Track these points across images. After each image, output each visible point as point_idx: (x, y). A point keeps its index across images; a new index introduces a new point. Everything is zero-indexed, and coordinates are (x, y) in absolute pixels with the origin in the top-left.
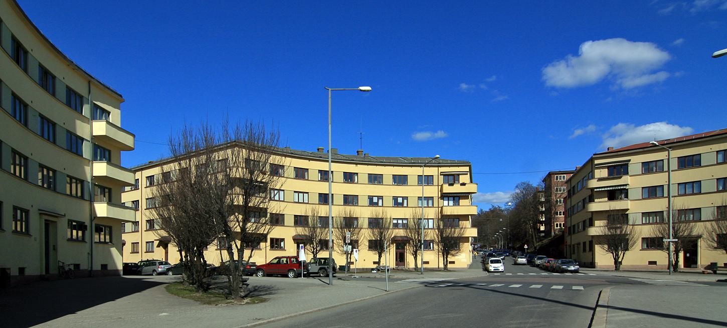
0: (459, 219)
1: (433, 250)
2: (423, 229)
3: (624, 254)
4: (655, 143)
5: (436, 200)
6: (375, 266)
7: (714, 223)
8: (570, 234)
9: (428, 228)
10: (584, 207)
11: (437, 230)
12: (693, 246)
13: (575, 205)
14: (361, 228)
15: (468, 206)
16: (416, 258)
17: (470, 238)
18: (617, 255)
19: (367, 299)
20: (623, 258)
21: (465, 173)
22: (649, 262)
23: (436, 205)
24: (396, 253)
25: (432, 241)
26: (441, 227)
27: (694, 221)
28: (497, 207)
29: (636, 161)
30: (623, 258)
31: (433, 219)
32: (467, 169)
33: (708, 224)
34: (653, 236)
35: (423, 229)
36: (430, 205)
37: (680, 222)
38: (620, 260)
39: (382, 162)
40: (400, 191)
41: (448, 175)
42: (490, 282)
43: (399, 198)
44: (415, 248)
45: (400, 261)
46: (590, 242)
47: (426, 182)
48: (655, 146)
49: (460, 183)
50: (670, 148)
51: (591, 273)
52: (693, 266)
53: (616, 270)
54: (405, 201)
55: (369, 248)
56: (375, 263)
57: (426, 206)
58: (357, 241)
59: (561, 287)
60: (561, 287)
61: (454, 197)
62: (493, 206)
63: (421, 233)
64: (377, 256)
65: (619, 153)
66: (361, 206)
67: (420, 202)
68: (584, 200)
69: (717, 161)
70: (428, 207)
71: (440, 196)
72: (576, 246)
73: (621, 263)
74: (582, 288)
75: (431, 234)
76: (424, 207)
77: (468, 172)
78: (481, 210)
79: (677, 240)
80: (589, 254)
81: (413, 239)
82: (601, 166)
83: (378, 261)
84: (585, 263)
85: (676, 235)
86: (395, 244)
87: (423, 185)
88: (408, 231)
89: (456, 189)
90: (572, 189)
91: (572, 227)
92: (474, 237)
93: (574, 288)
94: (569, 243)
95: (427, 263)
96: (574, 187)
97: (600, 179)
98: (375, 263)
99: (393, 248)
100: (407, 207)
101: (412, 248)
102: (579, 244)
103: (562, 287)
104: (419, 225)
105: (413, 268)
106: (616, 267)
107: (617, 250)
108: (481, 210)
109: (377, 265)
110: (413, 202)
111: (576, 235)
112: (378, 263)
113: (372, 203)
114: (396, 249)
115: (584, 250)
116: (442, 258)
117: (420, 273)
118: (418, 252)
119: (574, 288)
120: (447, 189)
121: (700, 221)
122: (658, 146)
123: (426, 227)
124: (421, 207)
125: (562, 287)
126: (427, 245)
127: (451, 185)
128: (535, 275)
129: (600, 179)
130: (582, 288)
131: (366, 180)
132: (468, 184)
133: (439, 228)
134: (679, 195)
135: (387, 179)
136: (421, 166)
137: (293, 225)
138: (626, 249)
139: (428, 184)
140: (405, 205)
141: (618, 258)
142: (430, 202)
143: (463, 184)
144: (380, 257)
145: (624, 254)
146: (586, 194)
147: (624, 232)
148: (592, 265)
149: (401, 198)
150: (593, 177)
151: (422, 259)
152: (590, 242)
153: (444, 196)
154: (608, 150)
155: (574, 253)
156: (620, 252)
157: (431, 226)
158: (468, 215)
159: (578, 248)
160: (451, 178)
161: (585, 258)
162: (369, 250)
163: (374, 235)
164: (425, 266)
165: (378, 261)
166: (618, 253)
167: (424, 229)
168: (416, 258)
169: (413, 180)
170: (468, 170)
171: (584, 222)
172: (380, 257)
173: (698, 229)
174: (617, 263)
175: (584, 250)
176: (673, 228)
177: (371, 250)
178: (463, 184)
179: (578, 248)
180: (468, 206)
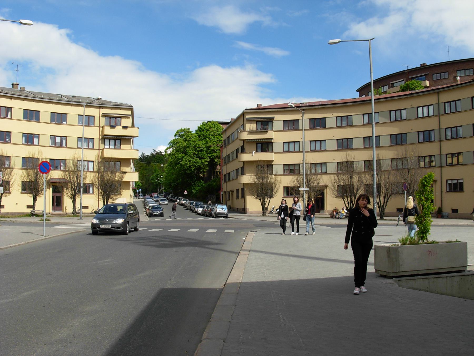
0: (120, 162)
1: (93, 194)
2: (82, 171)
3: (269, 201)
4: (292, 105)
5: (96, 141)
6: (29, 211)
7: (335, 176)
8: (225, 181)
9: (88, 171)
10: (237, 157)
11: (97, 174)
12: (321, 194)
13: (229, 154)
14: (13, 169)
15: (130, 150)
16: (74, 202)
17: (131, 183)
18: (264, 201)
19: (22, 244)
20: (268, 205)
21: (127, 117)
22: (397, 209)
23: (96, 146)
24: (53, 197)
25: (92, 184)
26: (102, 170)
27: (322, 174)
28: (158, 152)
29: (279, 119)
30: (268, 205)
31: (93, 161)
32: (129, 112)
33: (332, 176)
34: (293, 185)
35: (82, 171)
36: (91, 146)
37: (311, 174)
38: (266, 206)
39: (40, 98)
40: (58, 130)
41: (110, 117)
42: (169, 227)
43: (57, 138)
44: (73, 191)
45: (57, 205)
46: (242, 189)
47: (87, 123)
48: (291, 107)
49: (122, 125)
50: (304, 110)
51: (242, 217)
52: (321, 211)
53: (263, 215)
54: (64, 142)
55: (22, 190)
56: (28, 207)
57: (86, 147)
58: (8, 182)
59: (214, 231)
60: (214, 231)
61: (115, 140)
62: (155, 151)
63: (80, 176)
64: (32, 199)
65: (265, 110)
66: (363, 161)
67: (80, 143)
68: (237, 150)
69: (337, 125)
70: (88, 149)
71: (100, 137)
72: (230, 192)
73: (267, 208)
74: (232, 231)
75: (90, 178)
76: (84, 149)
77: (130, 115)
78: (143, 154)
79: (309, 189)
80: (241, 200)
81: (71, 182)
82: (250, 120)
83: (32, 204)
84: (238, 209)
85: (308, 185)
86: (51, 189)
87: (84, 125)
88: (67, 173)
89: (118, 131)
90: (227, 139)
91: (227, 175)
92: (135, 182)
93: (226, 231)
94: (224, 190)
95: (86, 207)
96: (229, 138)
97: (251, 132)
98: (28, 207)
99: (49, 192)
100: (66, 147)
101: (70, 191)
102: (233, 191)
103: (217, 230)
104: (78, 167)
105: (71, 213)
106: (263, 213)
107: (264, 199)
108: (143, 154)
109: (32, 209)
110: (72, 142)
111: (230, 182)
112: (33, 207)
113: (54, 144)
114: (52, 192)
115: (238, 197)
116: (102, 202)
117: (79, 218)
118: (77, 196)
119: (226, 231)
120: (108, 131)
121: (326, 173)
122: (294, 108)
123: (86, 169)
124: (81, 148)
125: (217, 230)
126: (86, 189)
127: (113, 127)
128: (192, 220)
129: (251, 132)
130: (232, 231)
131: (21, 116)
132: (130, 127)
133: (99, 171)
134: (311, 151)
135: (45, 117)
136: (81, 106)
137: (21, 167)
138: (271, 197)
139: (89, 124)
140: (64, 145)
141: (265, 204)
142: (91, 144)
143: (125, 128)
144: (35, 199)
145: (269, 201)
146: (238, 144)
147: (269, 181)
148: (243, 211)
149: (60, 138)
150: (244, 130)
151: (81, 204)
152: (242, 189)
153: (105, 138)
154: (258, 106)
155: (229, 200)
156: (266, 199)
157: (91, 169)
158: (130, 159)
159: (232, 194)
160: (113, 120)
161: (238, 204)
162: (22, 193)
163: (28, 175)
164: (84, 211)
165: (32, 204)
166: (265, 200)
167: (84, 171)
168: (74, 202)
169: (45, 117)
170: (130, 114)
171: (237, 170)
172: (35, 199)
173: (324, 180)
174: (264, 209)
175: (238, 197)
176: (307, 179)
177: (25, 193)
178: (125, 128)
179: (232, 194)
180: (130, 150)
